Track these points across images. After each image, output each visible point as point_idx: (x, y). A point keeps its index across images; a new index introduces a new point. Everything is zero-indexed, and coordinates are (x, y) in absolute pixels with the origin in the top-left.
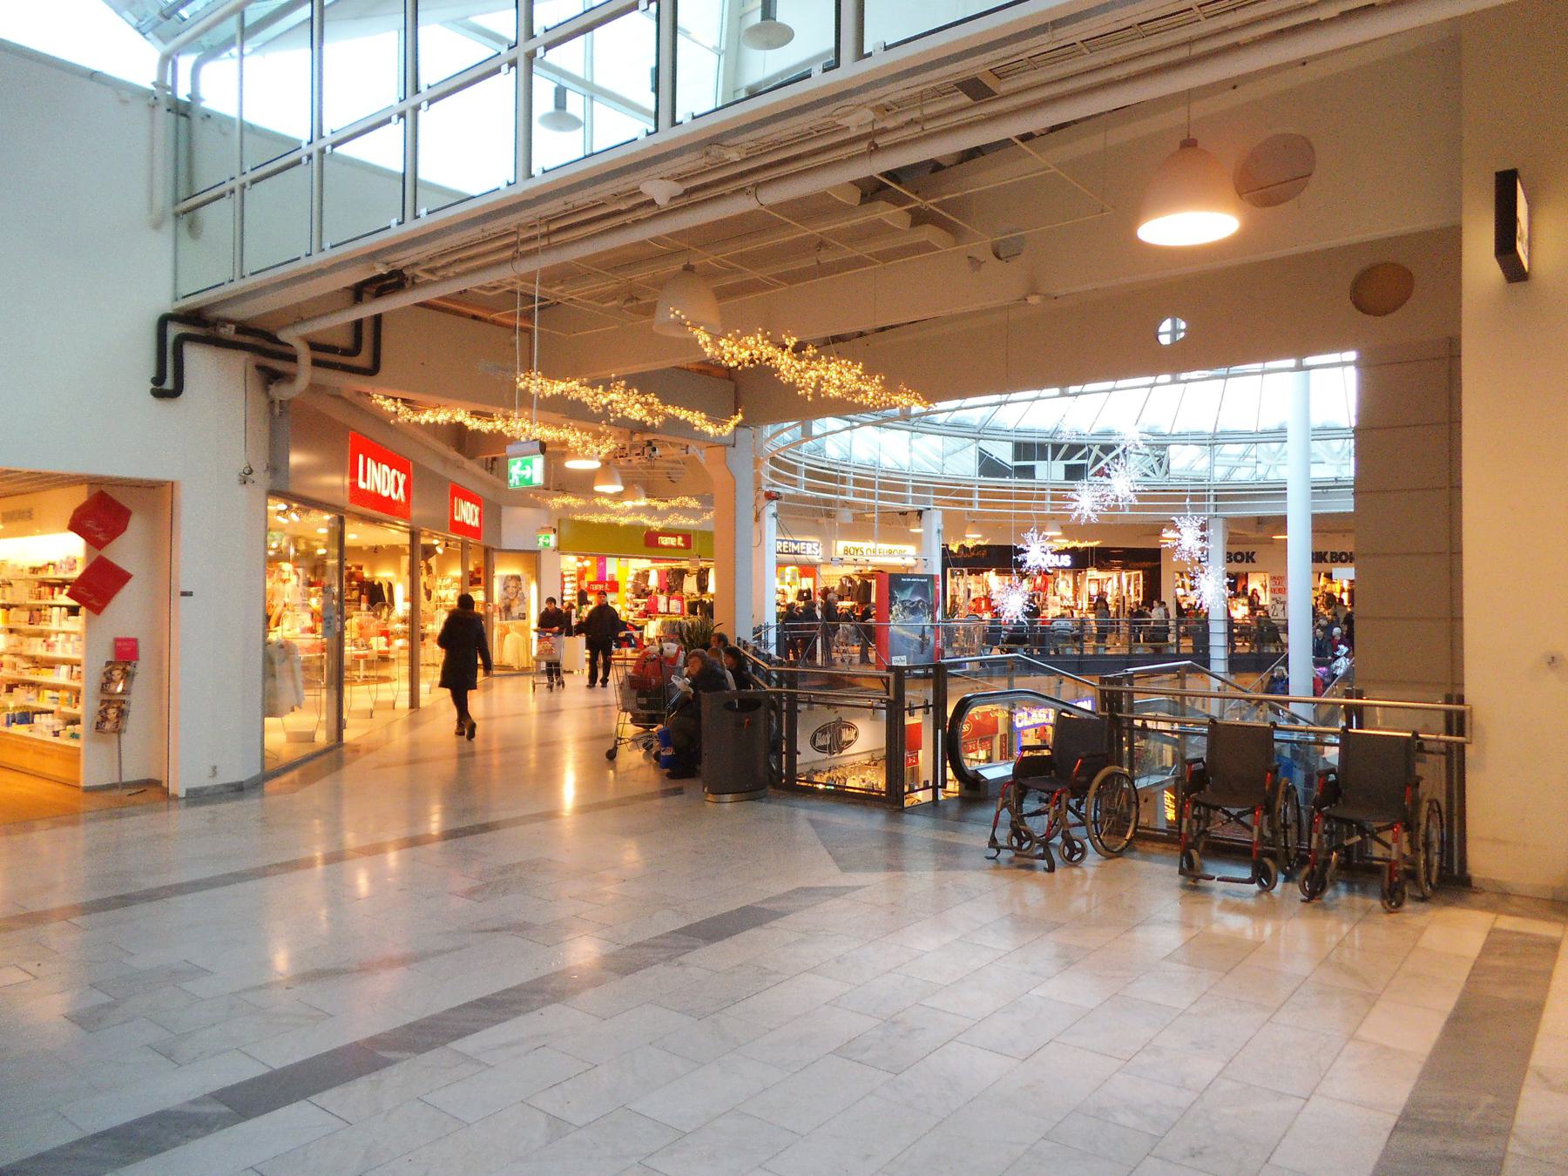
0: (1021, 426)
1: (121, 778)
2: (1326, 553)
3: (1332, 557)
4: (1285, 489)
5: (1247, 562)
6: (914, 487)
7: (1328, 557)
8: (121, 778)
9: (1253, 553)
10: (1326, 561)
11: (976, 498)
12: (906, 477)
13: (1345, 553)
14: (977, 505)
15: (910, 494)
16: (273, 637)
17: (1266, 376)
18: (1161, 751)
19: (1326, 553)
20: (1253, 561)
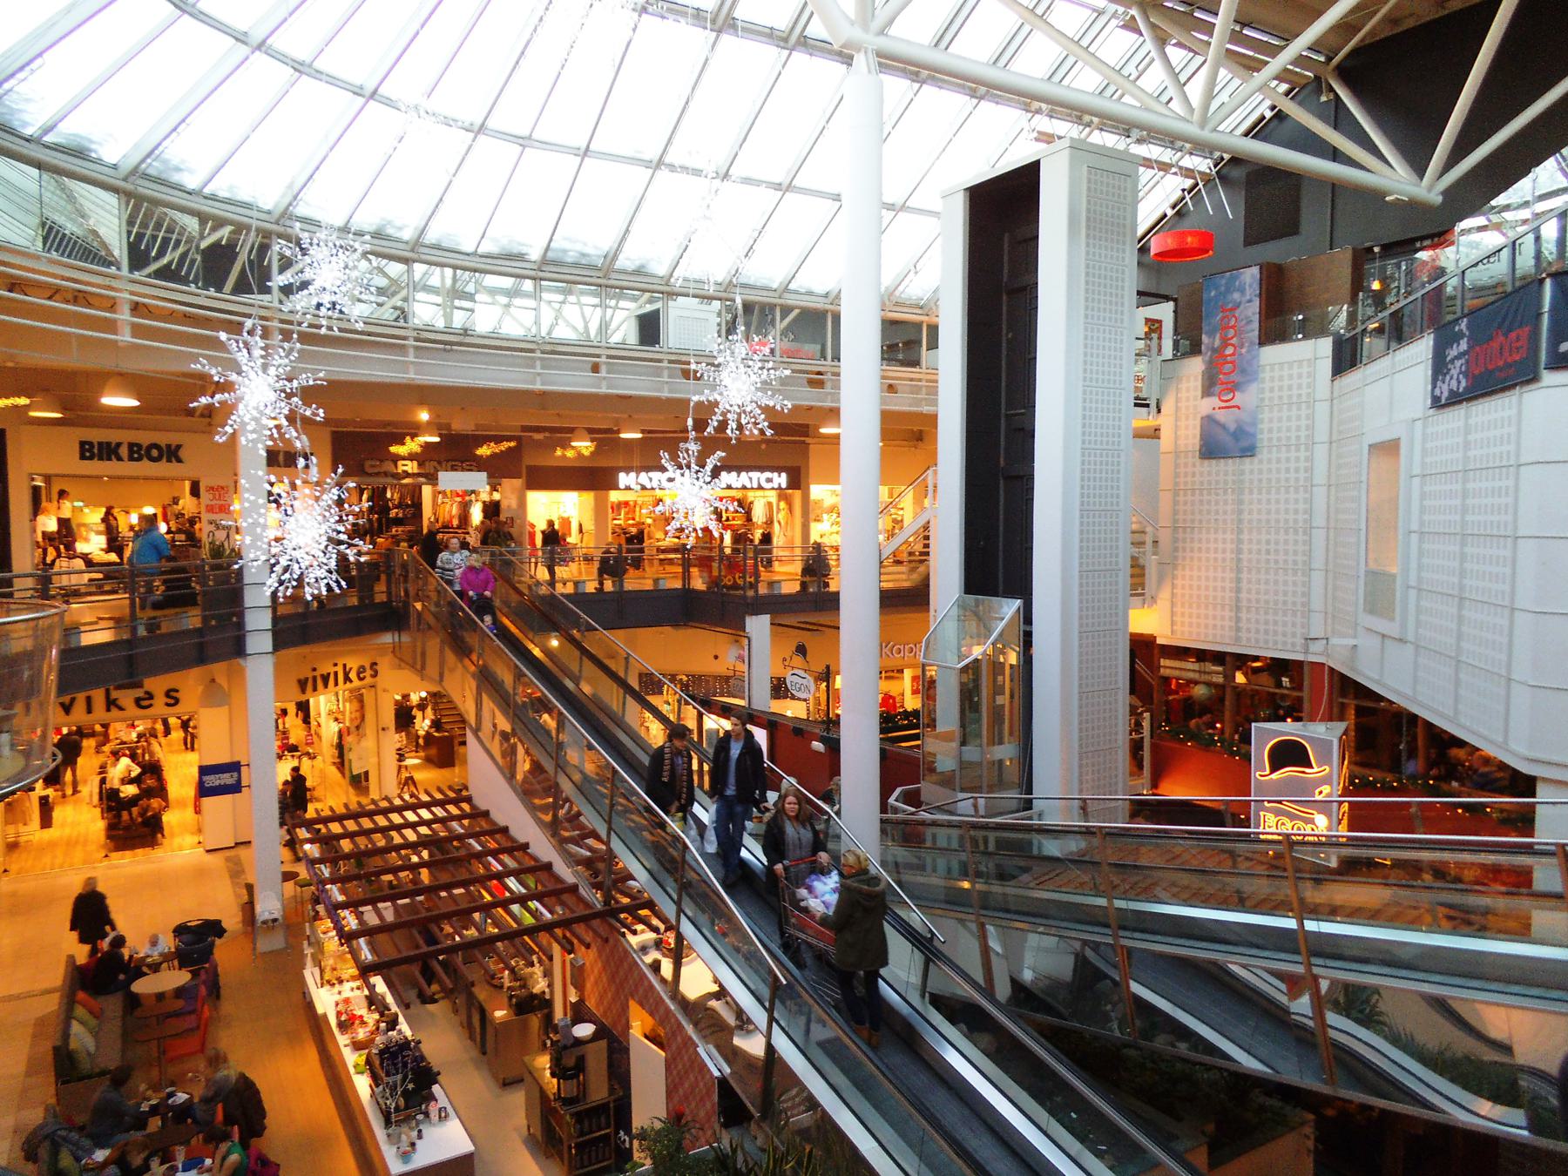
0: (219, 187)
1: (19, 576)
2: (119, 445)
3: (131, 452)
4: (936, 381)
5: (169, 460)
6: (416, 348)
7: (124, 451)
8: (19, 576)
9: (179, 447)
10: (119, 459)
11: (124, 315)
12: (597, 351)
13: (155, 446)
14: (127, 330)
15: (411, 358)
16: (1018, 603)
17: (799, 57)
18: (551, 912)
19: (119, 445)
20: (179, 461)
